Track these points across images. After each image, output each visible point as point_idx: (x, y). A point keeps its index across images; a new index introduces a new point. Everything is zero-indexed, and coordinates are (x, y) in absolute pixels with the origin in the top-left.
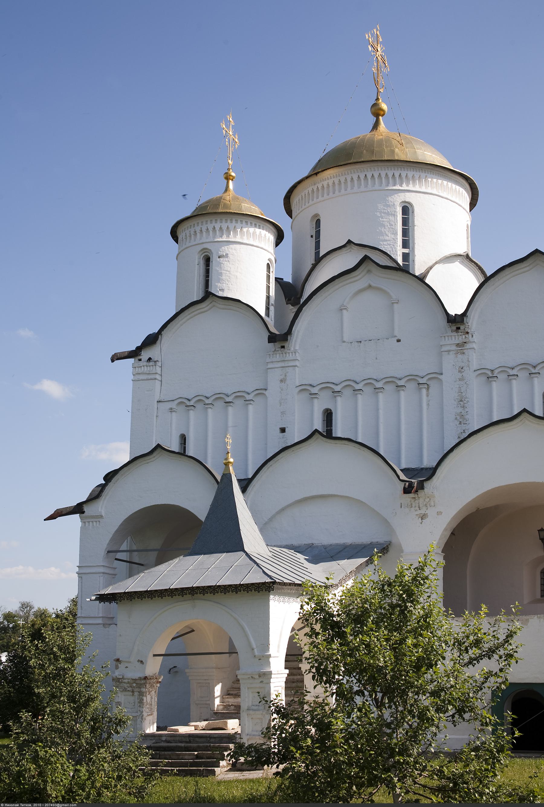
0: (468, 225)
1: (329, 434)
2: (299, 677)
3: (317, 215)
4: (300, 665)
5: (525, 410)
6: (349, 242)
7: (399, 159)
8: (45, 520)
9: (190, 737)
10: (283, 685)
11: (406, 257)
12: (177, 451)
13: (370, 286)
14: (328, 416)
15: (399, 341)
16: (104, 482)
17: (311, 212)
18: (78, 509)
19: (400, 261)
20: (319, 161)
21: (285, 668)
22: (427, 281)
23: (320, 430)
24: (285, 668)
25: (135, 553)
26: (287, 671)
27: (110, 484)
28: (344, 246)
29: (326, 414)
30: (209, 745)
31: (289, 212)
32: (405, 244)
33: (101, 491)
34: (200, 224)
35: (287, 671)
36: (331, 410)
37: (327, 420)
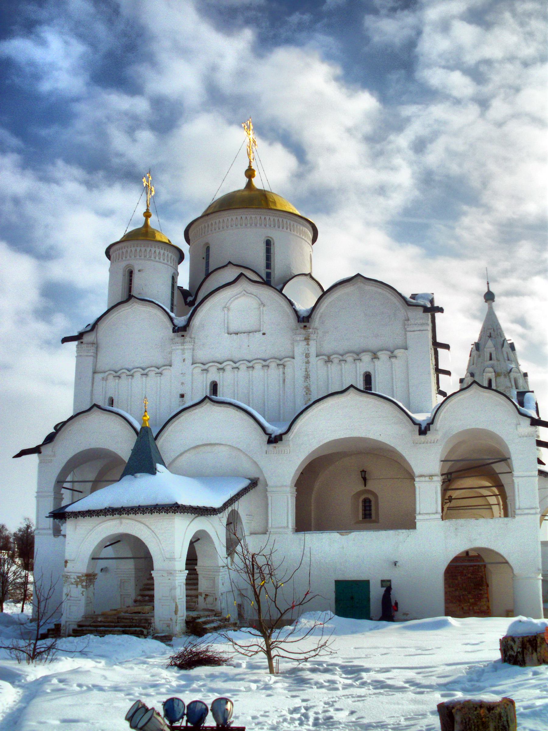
2: (194, 576)
3: (207, 243)
4: (196, 567)
5: (352, 386)
8: (14, 457)
10: (184, 581)
14: (214, 387)
15: (264, 334)
18: (36, 450)
19: (264, 276)
20: (209, 206)
21: (186, 569)
22: (283, 292)
23: (208, 395)
24: (186, 569)
26: (187, 572)
27: (60, 433)
29: (213, 385)
30: (131, 624)
31: (188, 240)
35: (187, 572)
36: (216, 382)
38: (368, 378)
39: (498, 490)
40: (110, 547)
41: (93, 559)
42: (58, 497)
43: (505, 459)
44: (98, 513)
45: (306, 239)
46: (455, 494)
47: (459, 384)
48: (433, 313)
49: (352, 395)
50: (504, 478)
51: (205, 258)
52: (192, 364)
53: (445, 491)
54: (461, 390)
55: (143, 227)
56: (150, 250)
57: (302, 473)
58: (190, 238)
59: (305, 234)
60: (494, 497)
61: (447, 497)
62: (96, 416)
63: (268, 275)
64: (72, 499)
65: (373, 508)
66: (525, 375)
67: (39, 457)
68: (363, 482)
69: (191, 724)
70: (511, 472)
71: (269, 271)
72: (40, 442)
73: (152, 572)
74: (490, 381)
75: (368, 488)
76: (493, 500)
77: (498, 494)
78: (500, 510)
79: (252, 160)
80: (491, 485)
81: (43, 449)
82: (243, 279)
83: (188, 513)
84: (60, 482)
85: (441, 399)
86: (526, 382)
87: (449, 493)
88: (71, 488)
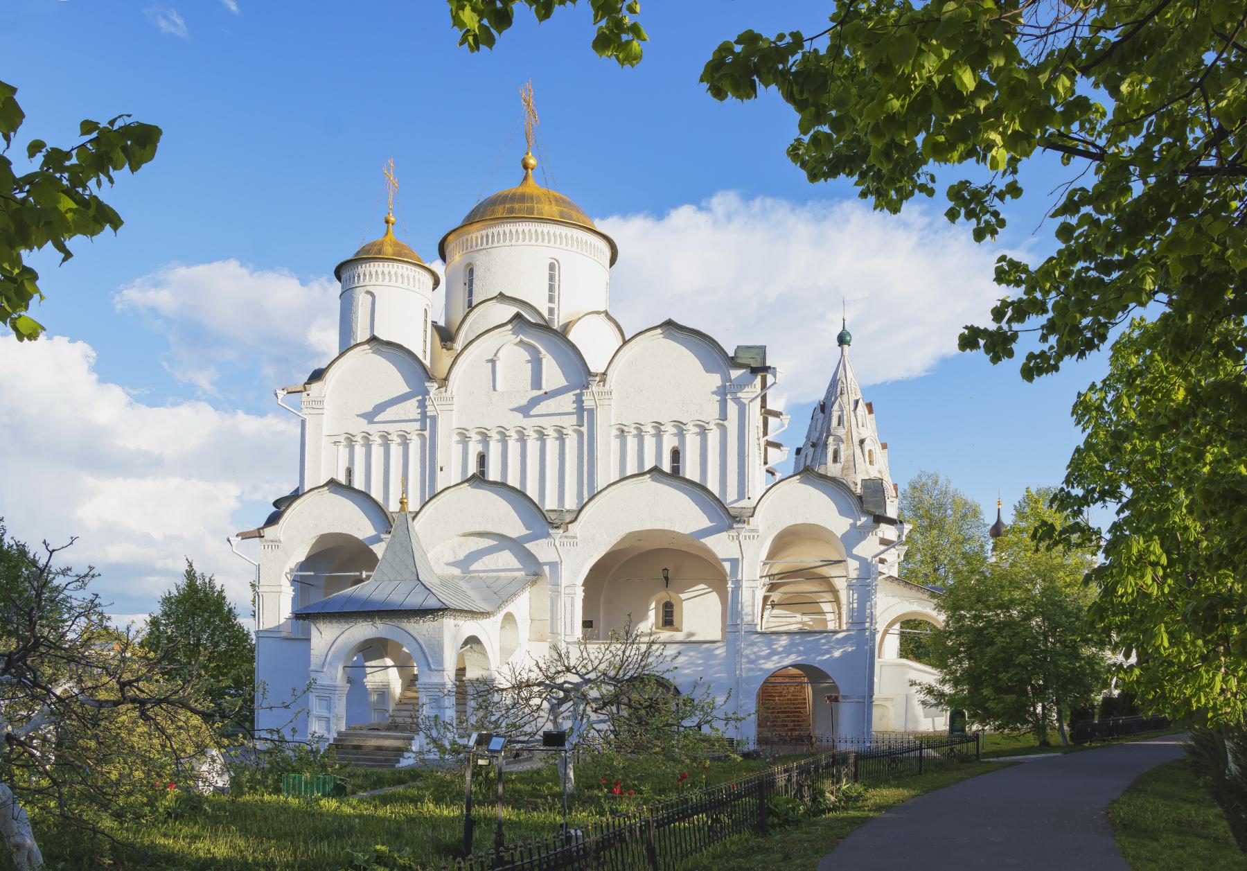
6: (501, 294)
11: (551, 311)
13: (521, 341)
22: (571, 337)
31: (443, 257)
32: (551, 299)
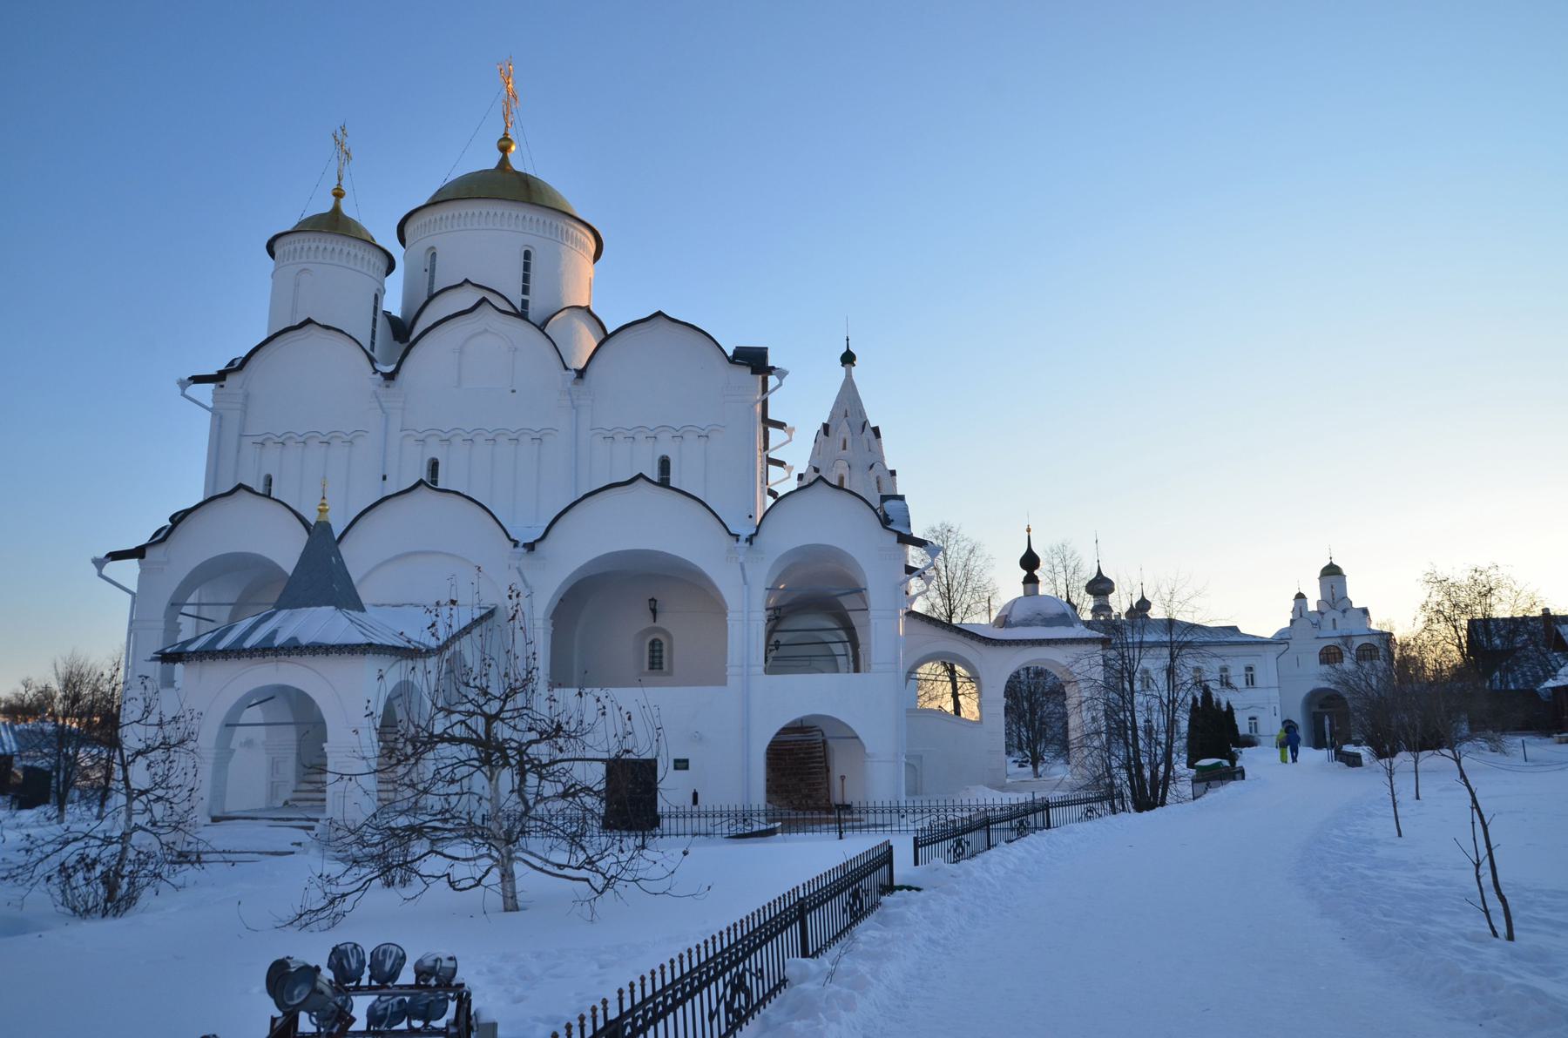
0: (590, 279)
1: (664, 483)
6: (467, 281)
7: (557, 207)
9: (963, 668)
12: (261, 492)
14: (434, 466)
16: (170, 524)
17: (429, 242)
18: (138, 553)
19: (519, 307)
20: (439, 190)
22: (546, 331)
23: (424, 479)
25: (205, 607)
28: (460, 285)
31: (402, 240)
33: (171, 530)
34: (301, 242)
37: (432, 470)
38: (665, 464)
39: (847, 634)
40: (257, 706)
41: (227, 725)
42: (172, 627)
43: (859, 591)
44: (238, 654)
45: (584, 254)
46: (783, 638)
47: (797, 482)
48: (765, 375)
49: (642, 490)
50: (856, 618)
51: (428, 271)
52: (401, 431)
53: (770, 633)
54: (799, 489)
55: (330, 212)
56: (341, 250)
57: (561, 600)
58: (407, 237)
59: (577, 242)
60: (840, 644)
61: (772, 642)
62: (244, 500)
63: (525, 303)
64: (197, 631)
65: (665, 654)
66: (893, 473)
67: (140, 564)
68: (651, 615)
69: (378, 982)
70: (867, 610)
71: (525, 297)
72: (144, 540)
73: (324, 745)
74: (841, 479)
75: (656, 625)
76: (838, 649)
77: (846, 639)
78: (849, 664)
79: (509, 125)
80: (836, 627)
81: (149, 553)
82: (485, 308)
83: (385, 654)
84: (176, 605)
85: (770, 501)
86: (894, 484)
87: (776, 636)
88: (195, 614)
